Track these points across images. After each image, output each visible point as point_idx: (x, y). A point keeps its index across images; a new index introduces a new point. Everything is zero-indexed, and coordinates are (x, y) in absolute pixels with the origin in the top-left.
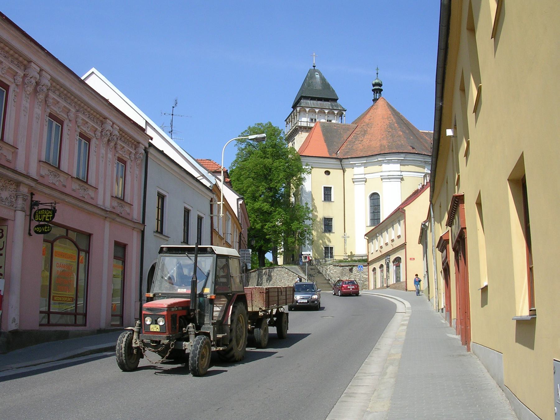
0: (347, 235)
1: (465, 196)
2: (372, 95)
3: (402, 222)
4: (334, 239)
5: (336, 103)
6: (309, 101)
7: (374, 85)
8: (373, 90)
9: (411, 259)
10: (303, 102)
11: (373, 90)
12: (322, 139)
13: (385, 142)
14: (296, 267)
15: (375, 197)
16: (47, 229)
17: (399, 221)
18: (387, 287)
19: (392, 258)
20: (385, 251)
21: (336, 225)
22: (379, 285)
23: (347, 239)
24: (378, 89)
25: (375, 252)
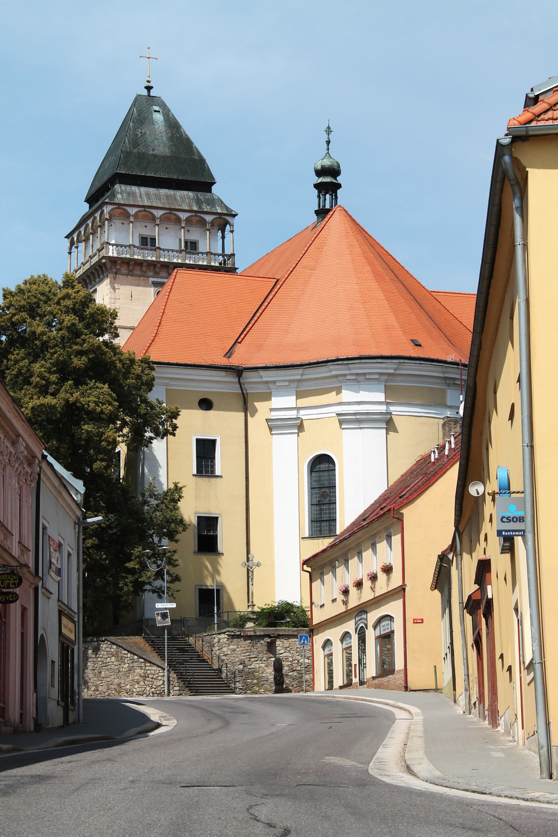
0: (255, 561)
3: (396, 539)
4: (228, 573)
5: (208, 195)
6: (135, 189)
7: (320, 173)
8: (316, 186)
9: (415, 621)
10: (122, 193)
11: (316, 186)
14: (138, 639)
15: (324, 466)
16: (12, 598)
17: (389, 537)
18: (362, 683)
19: (373, 616)
20: (354, 600)
21: (228, 537)
22: (339, 680)
23: (256, 570)
24: (328, 181)
25: (328, 604)
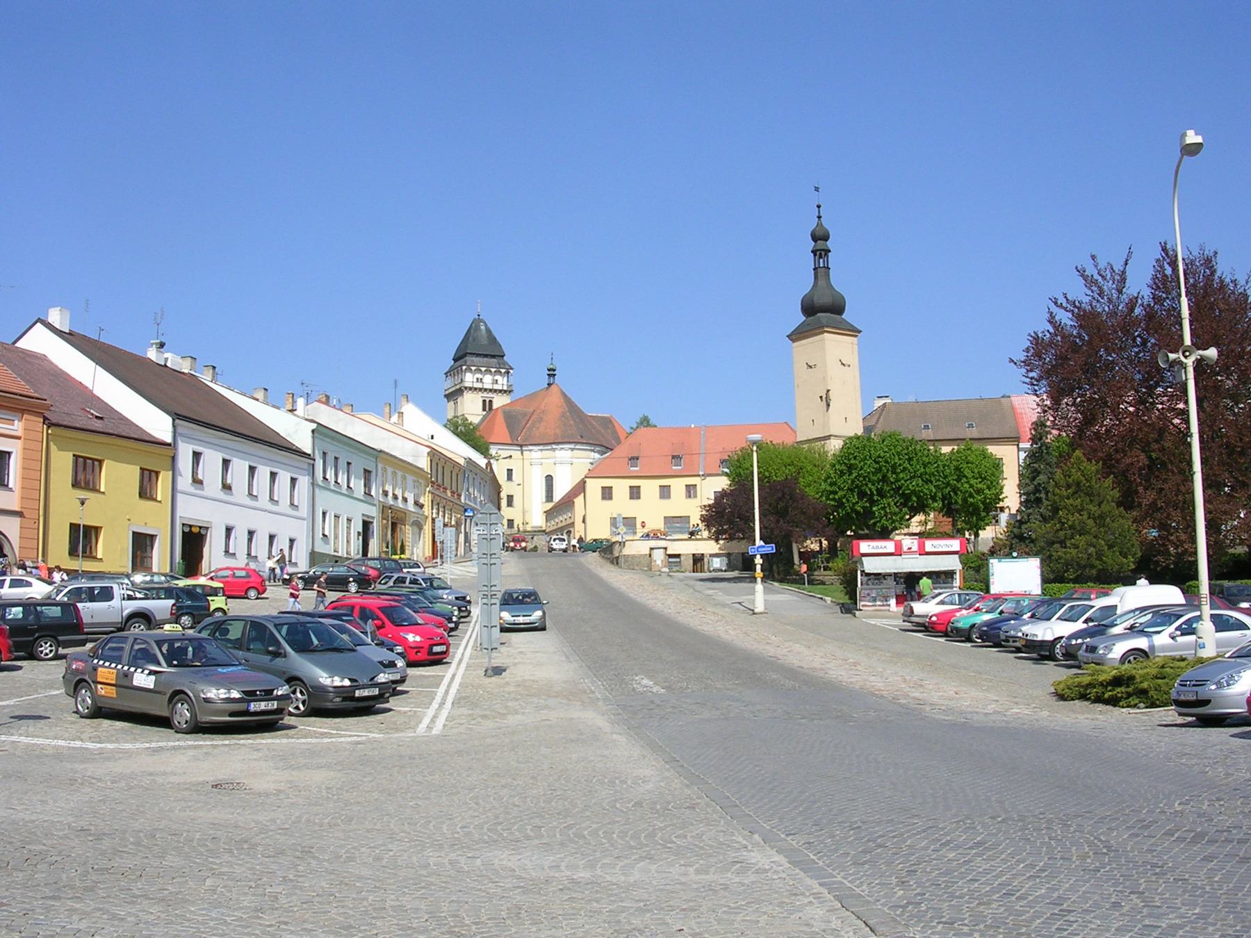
1: (614, 490)
2: (546, 380)
12: (504, 425)
13: (558, 431)
24: (552, 373)
